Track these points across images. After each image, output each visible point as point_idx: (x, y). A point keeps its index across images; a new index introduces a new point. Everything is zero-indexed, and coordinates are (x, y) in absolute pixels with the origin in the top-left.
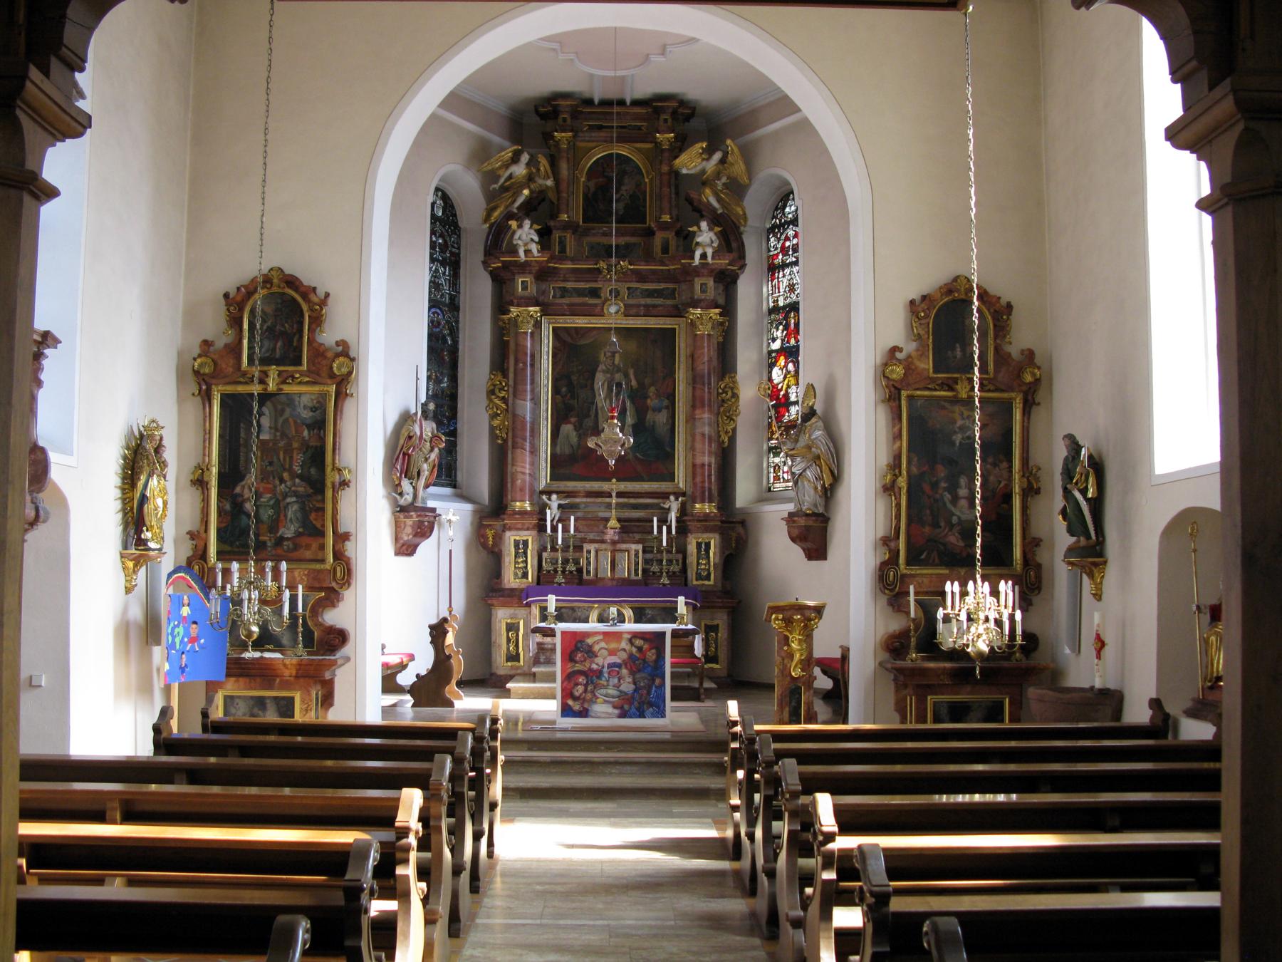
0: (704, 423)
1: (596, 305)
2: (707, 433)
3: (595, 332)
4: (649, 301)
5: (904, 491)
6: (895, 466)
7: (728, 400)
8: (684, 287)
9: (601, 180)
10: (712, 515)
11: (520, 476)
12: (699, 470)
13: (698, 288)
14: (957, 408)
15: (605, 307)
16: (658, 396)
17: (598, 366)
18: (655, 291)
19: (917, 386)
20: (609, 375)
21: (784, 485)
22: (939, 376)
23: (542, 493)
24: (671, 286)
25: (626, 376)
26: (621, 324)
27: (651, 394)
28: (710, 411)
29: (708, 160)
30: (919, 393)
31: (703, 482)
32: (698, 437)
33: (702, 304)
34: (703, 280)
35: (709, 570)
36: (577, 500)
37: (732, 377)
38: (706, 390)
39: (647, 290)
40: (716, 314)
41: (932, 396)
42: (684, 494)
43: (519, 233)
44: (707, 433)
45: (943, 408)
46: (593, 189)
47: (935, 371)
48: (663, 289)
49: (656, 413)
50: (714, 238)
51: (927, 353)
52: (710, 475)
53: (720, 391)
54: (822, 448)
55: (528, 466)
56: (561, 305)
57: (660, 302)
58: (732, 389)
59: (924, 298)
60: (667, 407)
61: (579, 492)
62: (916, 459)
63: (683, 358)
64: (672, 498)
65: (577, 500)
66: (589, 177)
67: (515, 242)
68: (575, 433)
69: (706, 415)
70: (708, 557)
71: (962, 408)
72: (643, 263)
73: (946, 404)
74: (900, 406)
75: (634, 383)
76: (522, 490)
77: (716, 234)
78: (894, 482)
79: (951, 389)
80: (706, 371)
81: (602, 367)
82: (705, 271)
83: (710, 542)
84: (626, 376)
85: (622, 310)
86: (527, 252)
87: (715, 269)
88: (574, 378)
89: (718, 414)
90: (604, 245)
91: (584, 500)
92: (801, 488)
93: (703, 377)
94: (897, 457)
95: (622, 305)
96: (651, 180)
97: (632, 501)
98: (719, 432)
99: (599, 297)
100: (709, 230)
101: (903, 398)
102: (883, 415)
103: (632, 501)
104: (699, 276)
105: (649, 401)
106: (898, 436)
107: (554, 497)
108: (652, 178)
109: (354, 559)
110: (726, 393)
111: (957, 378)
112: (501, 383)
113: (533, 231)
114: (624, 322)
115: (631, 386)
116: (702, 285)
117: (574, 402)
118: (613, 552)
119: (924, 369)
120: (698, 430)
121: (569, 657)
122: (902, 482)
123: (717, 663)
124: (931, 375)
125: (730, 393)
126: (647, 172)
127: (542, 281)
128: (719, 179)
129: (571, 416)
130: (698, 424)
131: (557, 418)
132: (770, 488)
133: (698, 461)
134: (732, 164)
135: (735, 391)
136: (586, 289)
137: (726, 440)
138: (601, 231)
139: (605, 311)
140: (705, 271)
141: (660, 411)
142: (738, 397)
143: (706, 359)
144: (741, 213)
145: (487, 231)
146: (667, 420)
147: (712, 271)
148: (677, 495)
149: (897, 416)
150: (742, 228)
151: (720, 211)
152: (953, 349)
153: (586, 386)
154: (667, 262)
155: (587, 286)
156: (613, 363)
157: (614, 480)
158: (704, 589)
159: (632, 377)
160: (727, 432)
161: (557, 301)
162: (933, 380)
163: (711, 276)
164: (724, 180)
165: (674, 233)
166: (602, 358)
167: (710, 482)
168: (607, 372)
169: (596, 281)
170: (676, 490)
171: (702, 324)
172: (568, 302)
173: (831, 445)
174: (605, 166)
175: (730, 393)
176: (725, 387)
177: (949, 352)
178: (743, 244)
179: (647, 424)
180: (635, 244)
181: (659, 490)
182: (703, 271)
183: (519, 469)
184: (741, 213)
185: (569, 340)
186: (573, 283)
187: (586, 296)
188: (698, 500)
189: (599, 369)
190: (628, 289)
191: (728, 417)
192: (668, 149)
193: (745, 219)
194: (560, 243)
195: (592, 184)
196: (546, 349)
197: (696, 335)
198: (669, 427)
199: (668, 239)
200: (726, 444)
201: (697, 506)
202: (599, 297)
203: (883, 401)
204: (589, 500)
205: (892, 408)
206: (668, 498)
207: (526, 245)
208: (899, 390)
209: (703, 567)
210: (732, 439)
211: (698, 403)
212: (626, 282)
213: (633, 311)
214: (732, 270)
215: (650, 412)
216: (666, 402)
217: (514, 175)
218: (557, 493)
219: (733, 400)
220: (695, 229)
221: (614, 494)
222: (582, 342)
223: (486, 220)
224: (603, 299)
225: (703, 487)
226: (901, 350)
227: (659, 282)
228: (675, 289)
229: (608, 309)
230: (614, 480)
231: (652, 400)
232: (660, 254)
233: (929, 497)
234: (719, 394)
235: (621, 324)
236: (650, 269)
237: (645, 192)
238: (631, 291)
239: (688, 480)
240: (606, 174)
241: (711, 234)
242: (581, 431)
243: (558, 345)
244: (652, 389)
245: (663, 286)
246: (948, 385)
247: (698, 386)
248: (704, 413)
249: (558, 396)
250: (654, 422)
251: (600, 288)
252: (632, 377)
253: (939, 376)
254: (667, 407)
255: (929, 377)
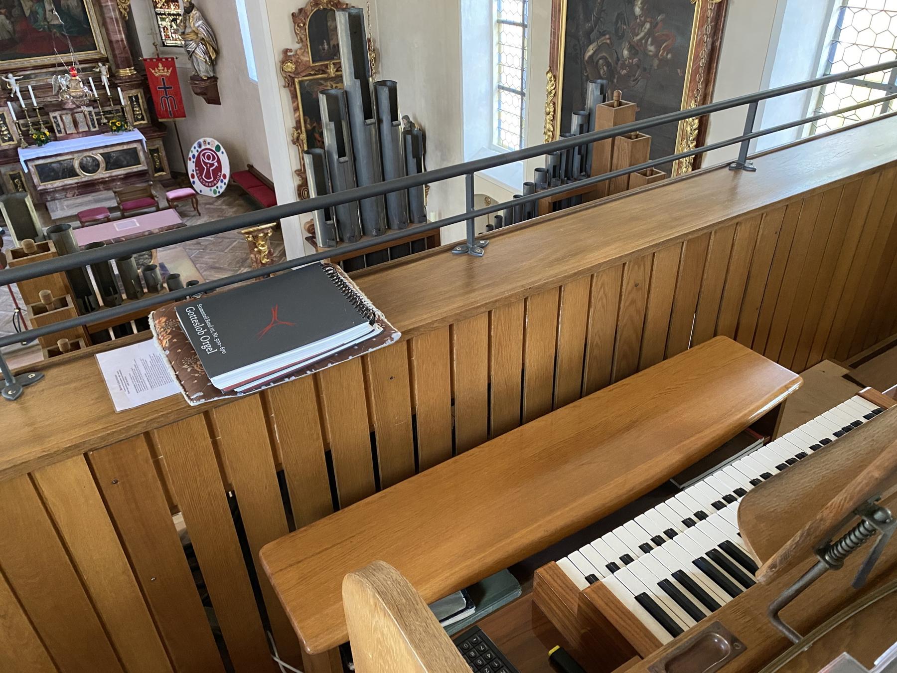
5: (305, 141)
6: (298, 127)
10: (134, 76)
14: (329, 84)
19: (304, 74)
21: (174, 42)
22: (317, 64)
30: (305, 78)
35: (142, 114)
41: (314, 79)
45: (322, 84)
47: (313, 62)
51: (307, 50)
54: (203, 33)
59: (301, 10)
62: (308, 120)
68: (8, 22)
70: (139, 106)
71: (332, 83)
73: (322, 82)
74: (295, 88)
78: (298, 138)
79: (324, 72)
83: (137, 95)
92: (195, 60)
94: (298, 122)
101: (296, 83)
102: (286, 95)
106: (296, 109)
107: (10, 75)
109: (16, 371)
111: (327, 64)
118: (72, 115)
119: (307, 61)
121: (24, 117)
122: (303, 136)
123: (163, 171)
124: (312, 65)
132: (163, 43)
148: (105, 61)
149: (294, 96)
152: (323, 44)
158: (142, 127)
162: (313, 68)
173: (210, 30)
177: (321, 46)
201: (121, 71)
203: (285, 87)
205: (290, 91)
208: (293, 79)
209: (138, 112)
210: (130, 13)
226: (291, 51)
233: (319, 141)
239: (107, 49)
246: (323, 71)
250: (68, 6)
253: (317, 64)
255: (310, 66)
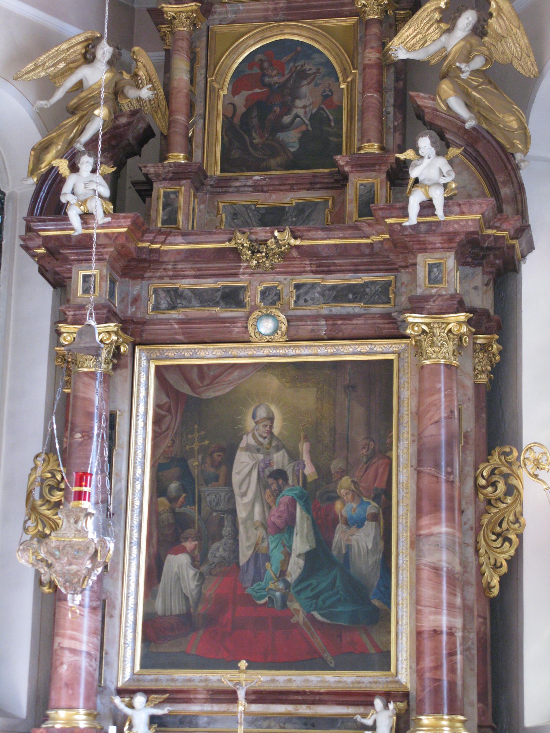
0: (438, 546)
1: (233, 320)
2: (444, 565)
3: (236, 374)
4: (337, 309)
7: (499, 499)
8: (404, 277)
9: (257, 90)
11: (67, 657)
12: (428, 644)
13: (422, 273)
15: (250, 323)
16: (357, 494)
17: (241, 439)
18: (350, 288)
20: (261, 457)
23: (121, 692)
24: (379, 278)
25: (294, 456)
26: (285, 356)
27: (343, 491)
28: (451, 521)
29: (450, 31)
31: (437, 667)
32: (426, 574)
33: (430, 306)
34: (434, 258)
36: (195, 708)
37: (506, 454)
38: (443, 477)
39: (334, 287)
40: (460, 323)
42: (406, 696)
43: (72, 180)
44: (444, 565)
46: (241, 109)
48: (366, 285)
49: (354, 528)
50: (446, 168)
52: (452, 654)
53: (483, 482)
55: (85, 637)
56: (166, 322)
57: (357, 310)
58: (506, 476)
60: (374, 517)
61: (195, 691)
63: (406, 419)
64: (378, 703)
65: (195, 708)
66: (235, 89)
67: (63, 199)
68: (192, 572)
69: (443, 529)
72: (320, 234)
75: (309, 470)
76: (72, 684)
77: (450, 162)
80: (443, 438)
81: (248, 440)
82: (436, 240)
84: (294, 456)
85: (284, 328)
86: (86, 217)
87: (455, 234)
88: (194, 463)
89: (478, 528)
90: (257, 209)
91: (207, 707)
93: (436, 449)
95: (282, 317)
96: (351, 86)
97: (304, 710)
98: (480, 565)
99: (240, 304)
100: (438, 154)
103: (304, 710)
104: (424, 250)
105: (338, 505)
107: (139, 700)
108: (353, 81)
110: (494, 485)
112: (54, 476)
113: (98, 178)
114: (292, 352)
115: (304, 476)
116: (431, 267)
117: (192, 511)
120: (427, 559)
125: (501, 487)
126: (344, 70)
127: (134, 278)
128: (467, 61)
129: (186, 539)
130: (426, 546)
131: (159, 541)
133: (427, 624)
134: (500, 38)
135: (514, 481)
136: (217, 290)
137: (495, 581)
138: (250, 183)
139: (251, 330)
140: (436, 240)
141: (360, 524)
142: (519, 494)
143: (443, 415)
144: (514, 125)
145: (33, 188)
146: (375, 544)
147: (450, 237)
148: (388, 696)
150: (519, 156)
151: (469, 125)
153: (217, 479)
154: (367, 229)
155: (219, 285)
156: (271, 433)
157: (243, 664)
159: (306, 458)
160: (496, 567)
161: (162, 316)
163: (448, 249)
164: (478, 63)
165: (384, 176)
166: (250, 424)
167: (452, 670)
168: (258, 451)
169: (235, 275)
170: (391, 687)
171: (432, 345)
172: (181, 317)
174: (266, 65)
175: (501, 487)
176: (492, 473)
178: (521, 188)
179: (335, 553)
180: (316, 204)
181: (356, 688)
182: (431, 239)
183: (67, 643)
184: (514, 125)
185: (186, 389)
186: (192, 281)
187: (217, 304)
188: (427, 707)
189: (243, 444)
190: (298, 287)
191: (498, 535)
192: (380, 21)
193: (526, 139)
194: (165, 206)
195: (240, 100)
196: (142, 409)
197: (422, 367)
198: (379, 556)
199: (372, 186)
200: (495, 592)
202: (240, 304)
204: (216, 707)
206: (372, 704)
207: (84, 202)
211: (426, 505)
212: (292, 273)
213: (306, 328)
214: (497, 238)
215: (340, 528)
216: (372, 507)
217: (85, 84)
218: (148, 692)
219: (509, 500)
220: (409, 154)
221: (241, 694)
222: (211, 394)
223: (32, 173)
224: (248, 308)
225: (437, 681)
227: (356, 271)
228: (389, 283)
229: (256, 327)
230: (243, 664)
231: (344, 504)
232: (356, 217)
234: (477, 488)
235: (285, 356)
236: (336, 245)
237: (340, 108)
238: (302, 291)
240: (267, 79)
241: (442, 163)
242: (204, 568)
243: (165, 399)
244: (346, 481)
245: (365, 278)
247: (426, 469)
248: (438, 523)
249: (163, 500)
250: (349, 547)
251: (244, 288)
252: (306, 458)
254: (374, 517)
